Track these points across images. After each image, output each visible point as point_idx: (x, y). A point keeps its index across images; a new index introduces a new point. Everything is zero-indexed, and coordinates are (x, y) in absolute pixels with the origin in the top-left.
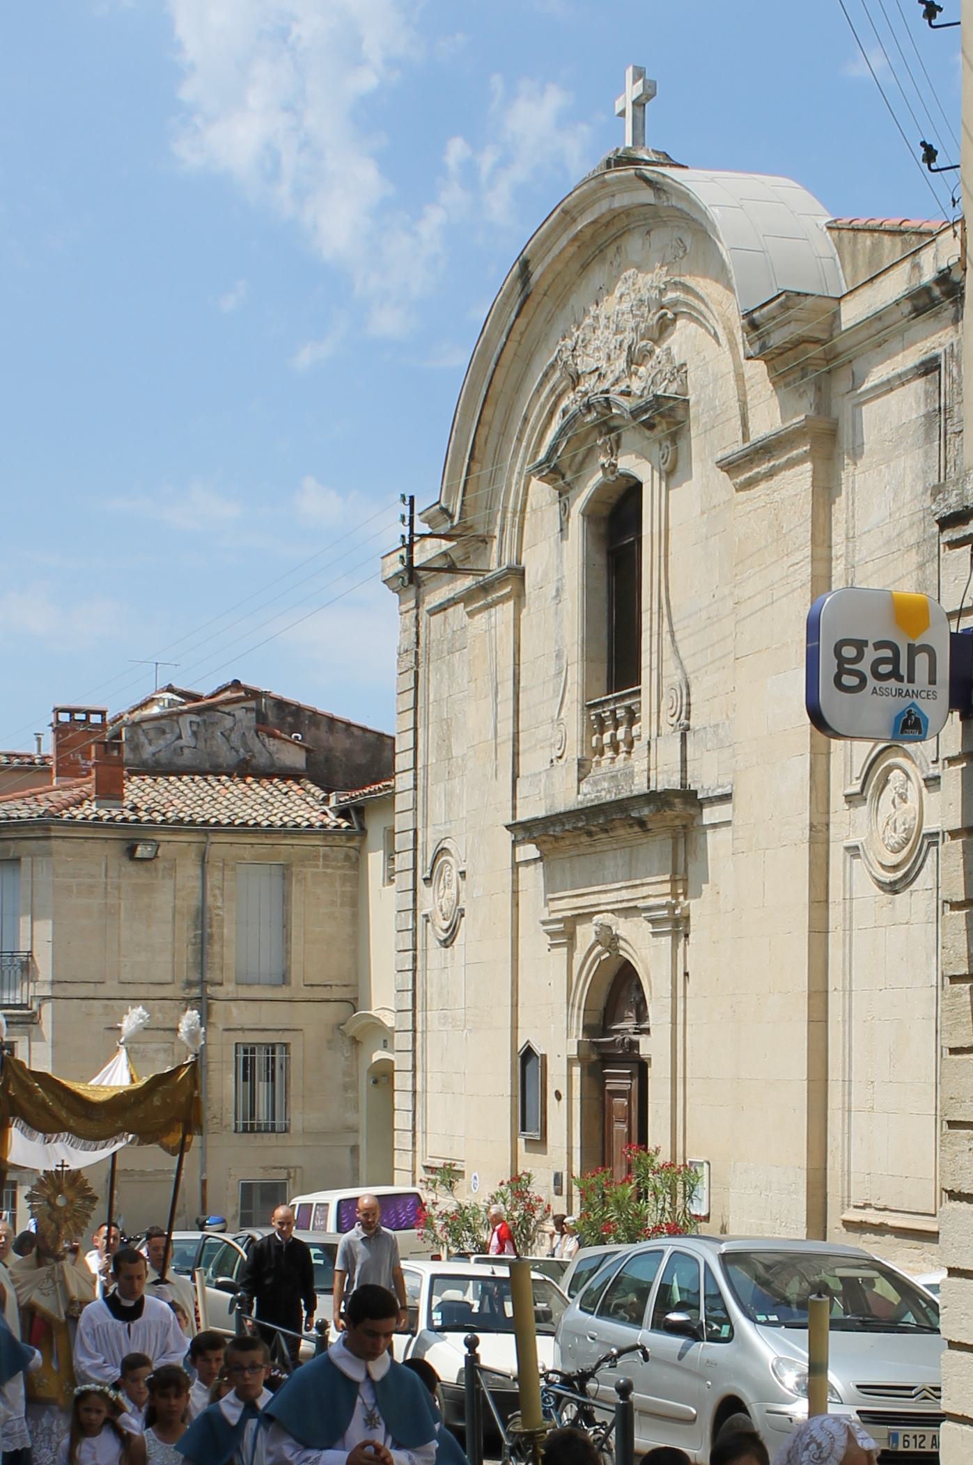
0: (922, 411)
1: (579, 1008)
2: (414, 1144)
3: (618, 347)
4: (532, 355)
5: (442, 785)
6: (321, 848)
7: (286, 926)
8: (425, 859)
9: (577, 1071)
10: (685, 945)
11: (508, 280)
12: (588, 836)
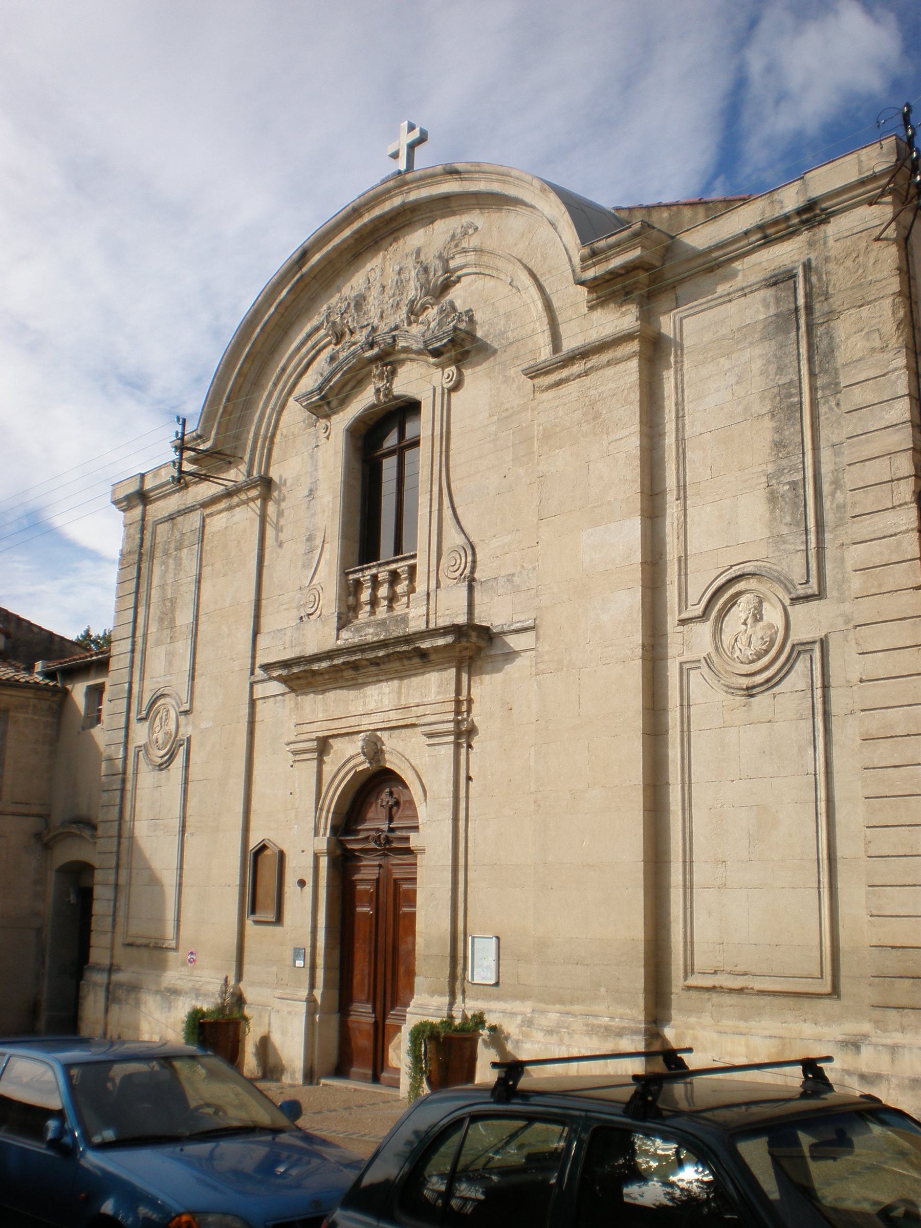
0: (772, 311)
1: (328, 812)
2: (114, 926)
3: (395, 305)
4: (291, 324)
5: (164, 647)
6: (32, 700)
7: (21, 803)
8: (140, 703)
9: (324, 862)
10: (468, 754)
11: (260, 298)
12: (354, 670)
